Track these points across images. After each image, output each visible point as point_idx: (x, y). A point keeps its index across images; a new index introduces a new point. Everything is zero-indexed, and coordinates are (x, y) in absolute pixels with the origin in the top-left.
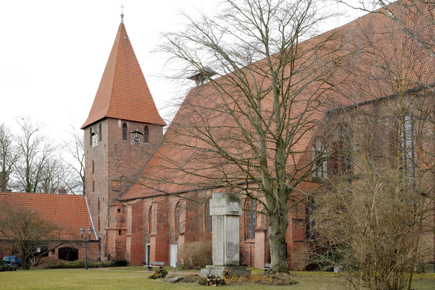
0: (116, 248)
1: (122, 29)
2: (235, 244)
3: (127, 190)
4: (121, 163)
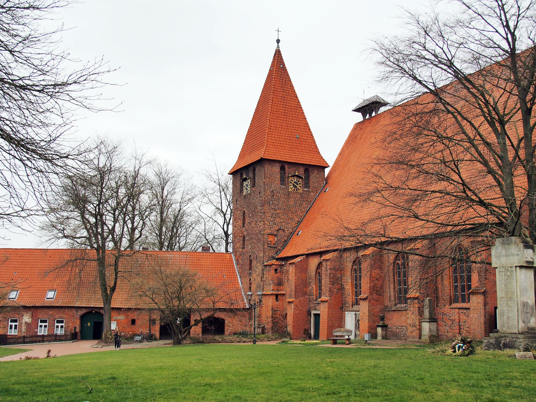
0: (272, 317)
1: (278, 54)
2: (531, 304)
3: (284, 247)
4: (278, 213)
